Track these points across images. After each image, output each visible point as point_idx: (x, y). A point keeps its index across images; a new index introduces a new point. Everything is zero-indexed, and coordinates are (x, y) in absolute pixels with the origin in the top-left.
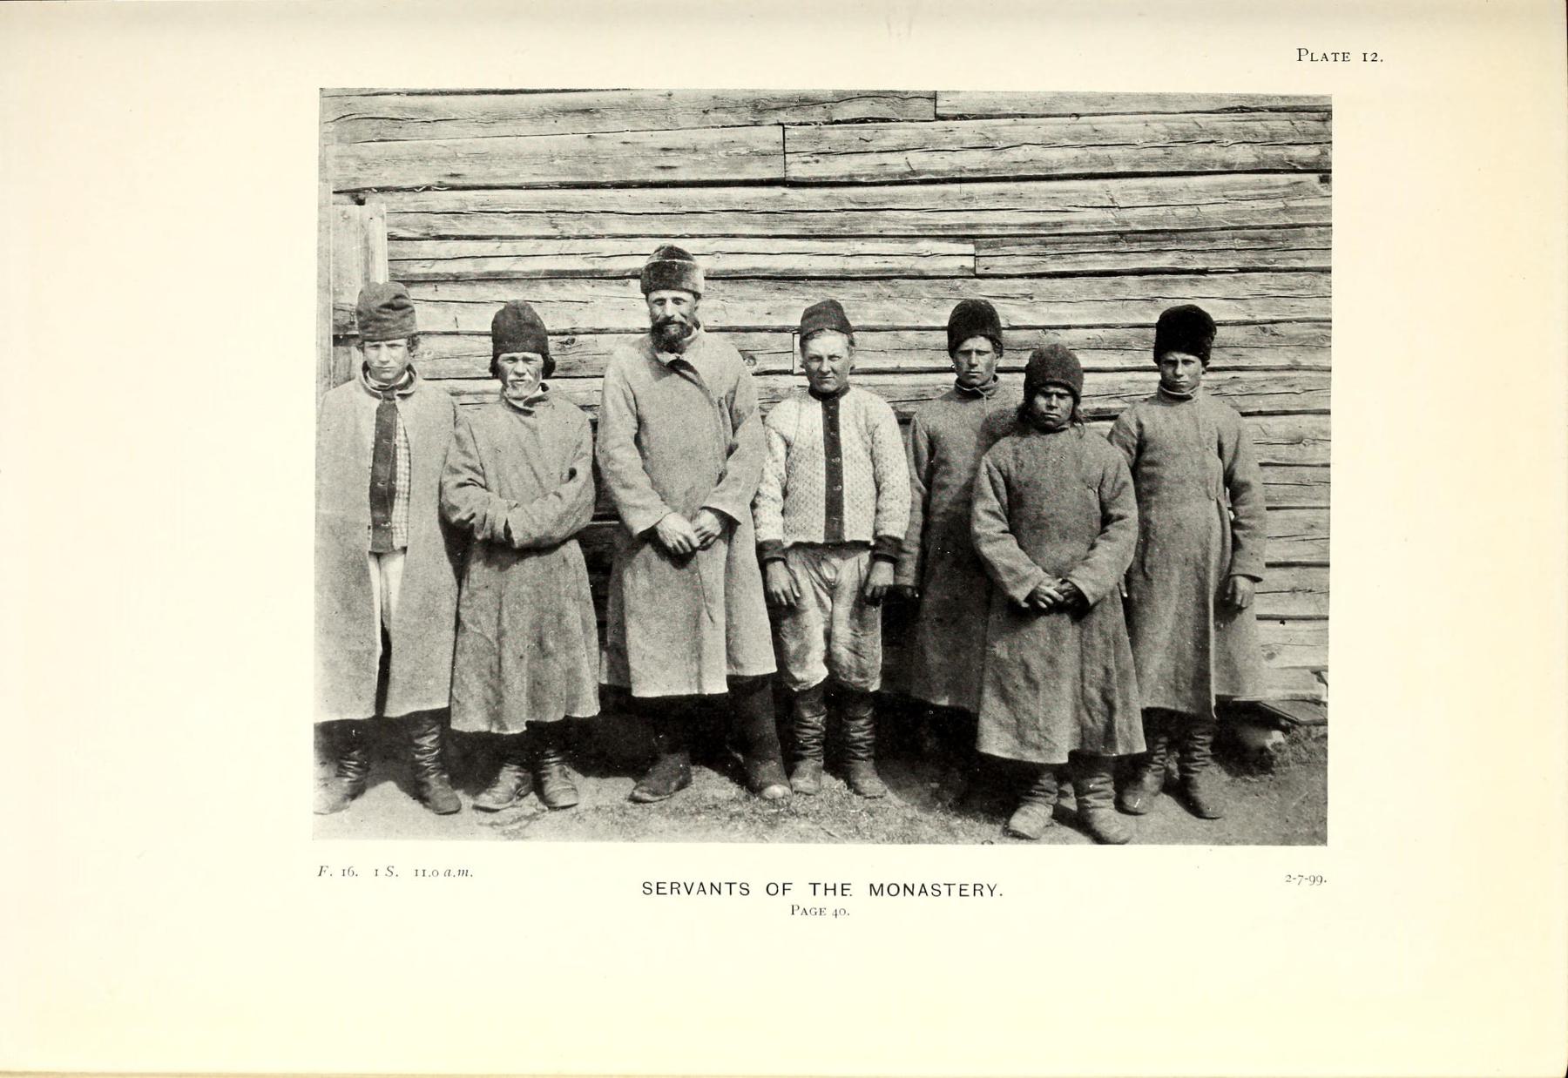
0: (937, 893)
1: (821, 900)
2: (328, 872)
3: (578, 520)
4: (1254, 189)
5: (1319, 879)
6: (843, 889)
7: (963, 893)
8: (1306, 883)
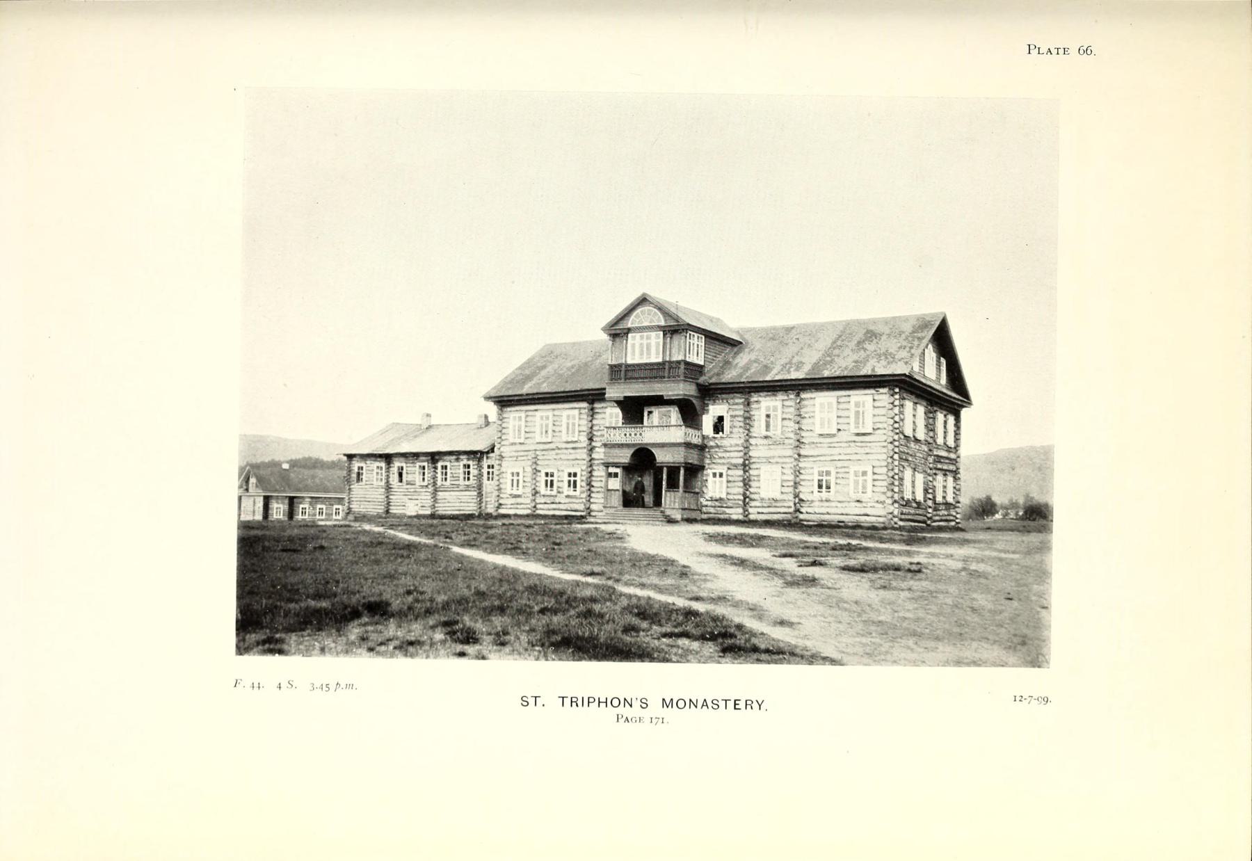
0: (716, 707)
3: (835, 371)
7: (737, 707)
8: (1034, 702)
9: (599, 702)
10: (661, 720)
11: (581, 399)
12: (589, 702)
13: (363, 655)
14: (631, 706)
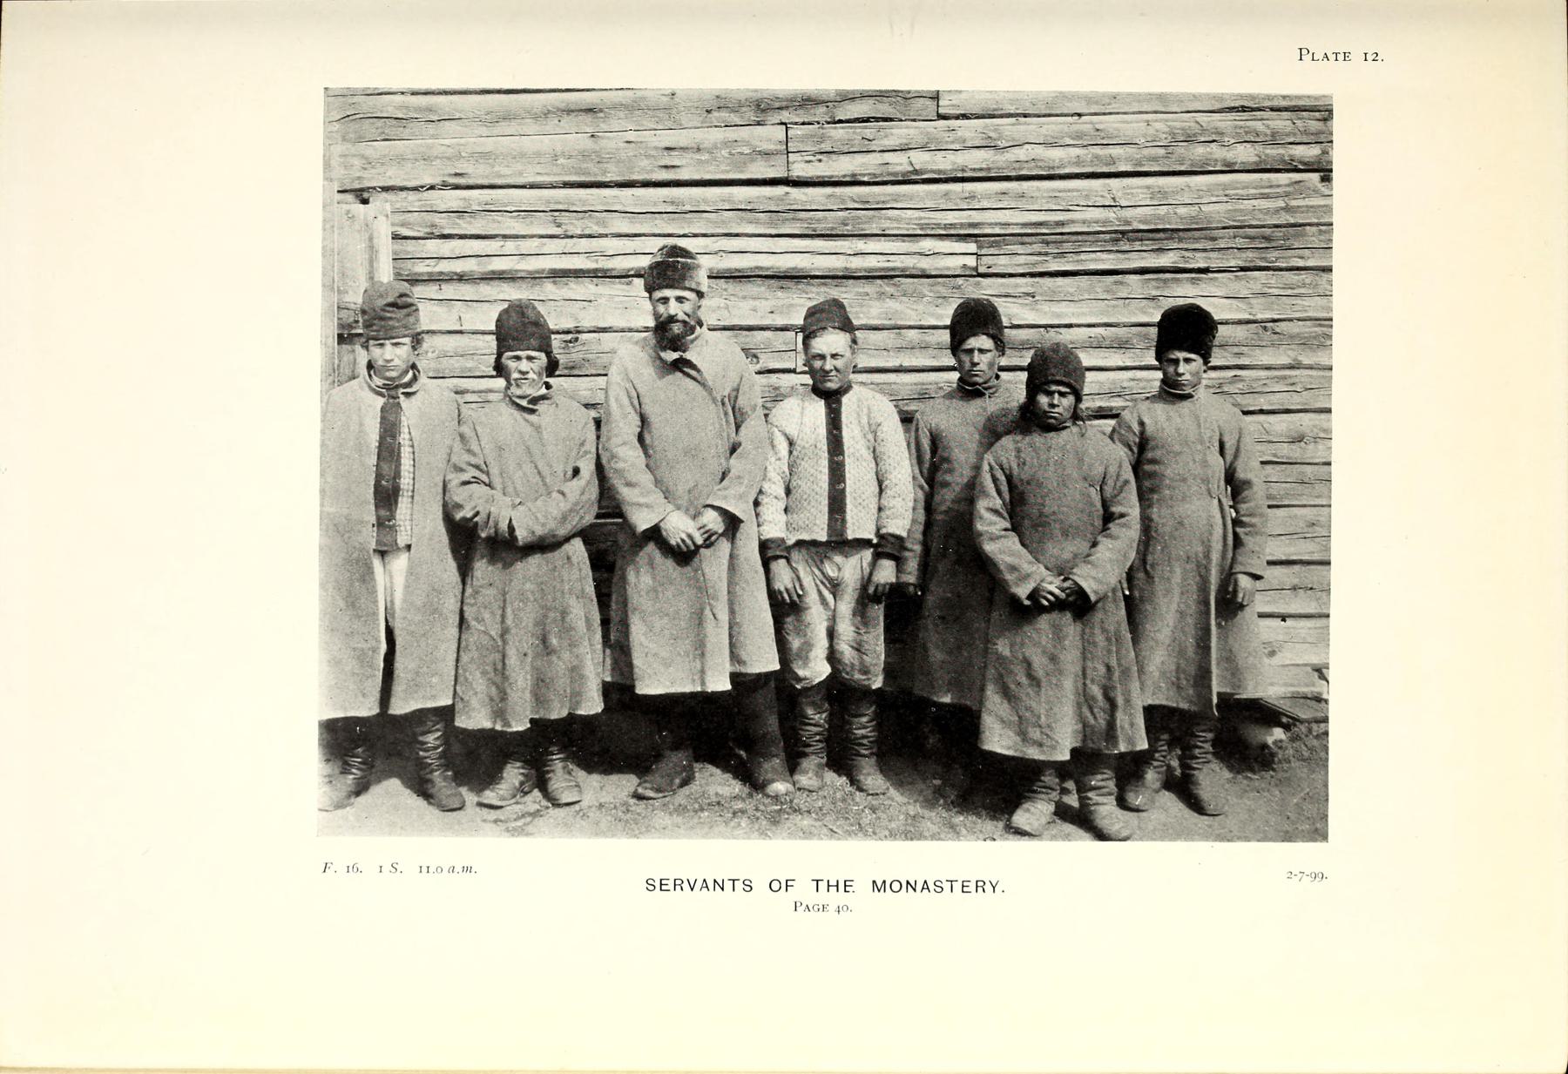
0: (939, 890)
1: (823, 896)
5: (1320, 875)
6: (661, 884)
7: (965, 889)
11: (936, 546)
13: (603, 825)
14: (723, 889)
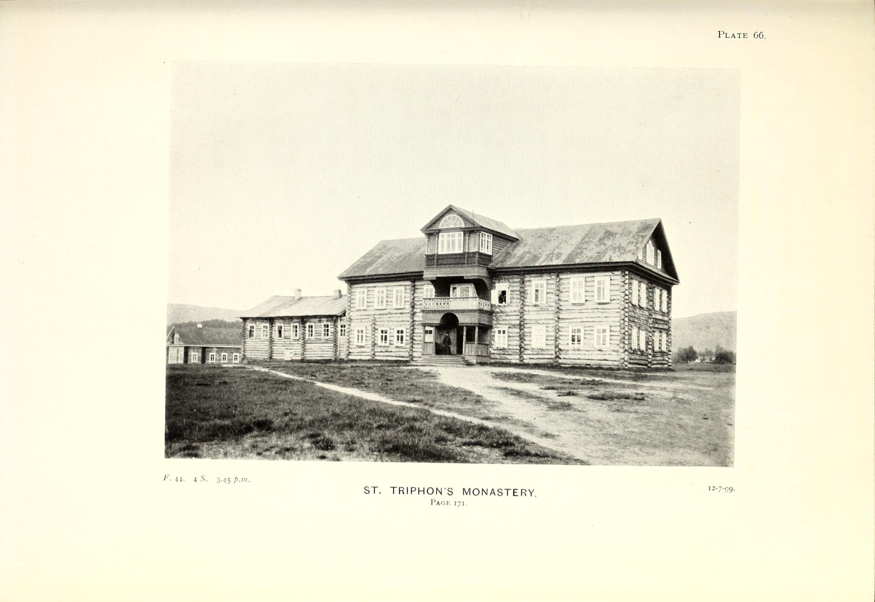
0: (501, 494)
2: (169, 479)
4: (646, 376)
7: (515, 494)
9: (419, 491)
10: (462, 503)
12: (412, 491)
14: (441, 493)
